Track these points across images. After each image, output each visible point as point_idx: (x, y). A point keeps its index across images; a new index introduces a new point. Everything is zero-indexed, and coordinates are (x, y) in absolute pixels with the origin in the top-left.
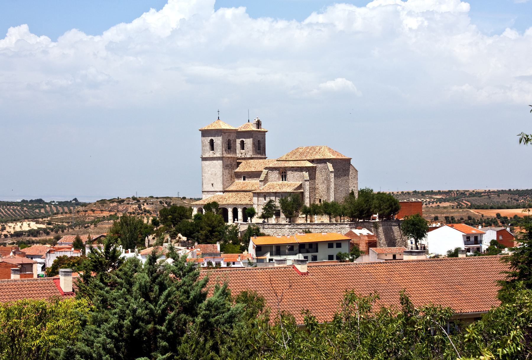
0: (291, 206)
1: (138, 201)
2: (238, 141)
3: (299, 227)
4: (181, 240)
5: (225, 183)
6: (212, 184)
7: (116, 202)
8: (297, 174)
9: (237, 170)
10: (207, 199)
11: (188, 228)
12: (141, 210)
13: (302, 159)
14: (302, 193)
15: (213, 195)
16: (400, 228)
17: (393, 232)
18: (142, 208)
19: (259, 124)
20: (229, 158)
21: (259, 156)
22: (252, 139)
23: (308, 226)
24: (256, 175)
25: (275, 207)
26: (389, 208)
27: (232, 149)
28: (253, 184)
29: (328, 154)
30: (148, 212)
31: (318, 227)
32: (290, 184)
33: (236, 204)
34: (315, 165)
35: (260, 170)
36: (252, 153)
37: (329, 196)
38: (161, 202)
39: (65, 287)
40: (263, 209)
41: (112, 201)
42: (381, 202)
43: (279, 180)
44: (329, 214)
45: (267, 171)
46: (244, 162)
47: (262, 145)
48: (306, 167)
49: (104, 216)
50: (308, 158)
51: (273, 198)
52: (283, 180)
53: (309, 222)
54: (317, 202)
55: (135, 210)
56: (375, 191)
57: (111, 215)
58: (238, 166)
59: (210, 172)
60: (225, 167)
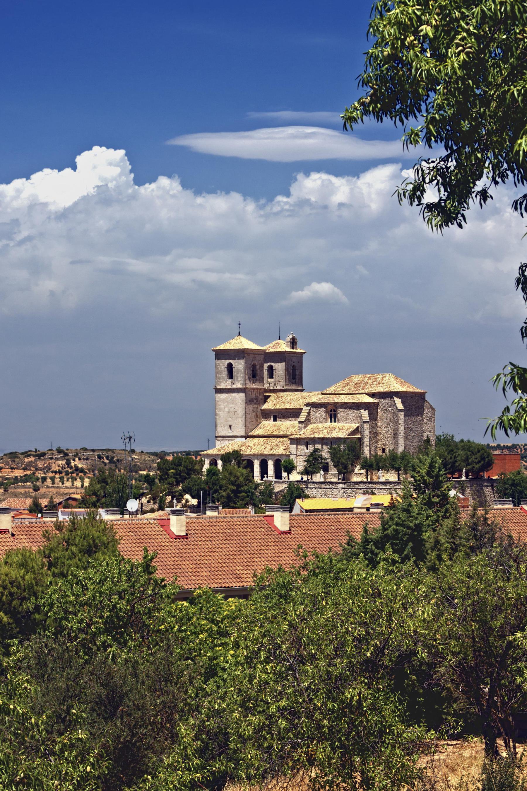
0: (346, 457)
1: (66, 455)
2: (266, 366)
3: (357, 486)
4: (190, 503)
5: (248, 425)
6: (230, 427)
7: (34, 456)
8: (352, 413)
9: (265, 407)
10: (222, 447)
11: (202, 487)
12: (71, 468)
13: (358, 392)
14: (360, 439)
15: (230, 442)
16: (493, 489)
17: (484, 493)
18: (73, 464)
20: (253, 389)
21: (294, 387)
22: (284, 364)
23: (370, 486)
24: (294, 413)
25: (322, 459)
26: (479, 462)
27: (257, 378)
28: (288, 426)
29: (396, 385)
30: (82, 470)
31: (383, 487)
32: (342, 428)
33: (266, 455)
34: (376, 401)
35: (297, 406)
36: (284, 384)
38: (100, 457)
39: (281, 525)
40: (305, 461)
41: (27, 454)
42: (469, 453)
43: (326, 421)
44: (398, 470)
45: (309, 408)
46: (273, 396)
47: (297, 372)
48: (365, 403)
49: (16, 477)
50: (367, 391)
51: (318, 446)
52: (331, 422)
53: (369, 480)
54: (380, 453)
55: (62, 468)
56: (457, 439)
57: (26, 475)
58: (265, 402)
59: (226, 410)
60: (249, 401)
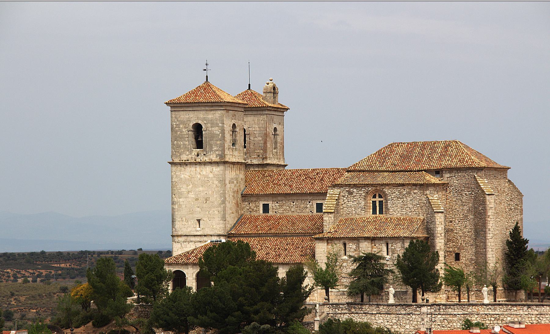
6: (199, 221)
19: (274, 91)
37: (170, 264)
50: (426, 167)
52: (374, 212)
59: (192, 195)
